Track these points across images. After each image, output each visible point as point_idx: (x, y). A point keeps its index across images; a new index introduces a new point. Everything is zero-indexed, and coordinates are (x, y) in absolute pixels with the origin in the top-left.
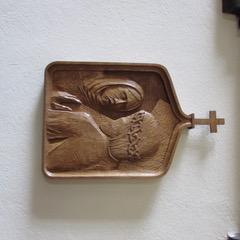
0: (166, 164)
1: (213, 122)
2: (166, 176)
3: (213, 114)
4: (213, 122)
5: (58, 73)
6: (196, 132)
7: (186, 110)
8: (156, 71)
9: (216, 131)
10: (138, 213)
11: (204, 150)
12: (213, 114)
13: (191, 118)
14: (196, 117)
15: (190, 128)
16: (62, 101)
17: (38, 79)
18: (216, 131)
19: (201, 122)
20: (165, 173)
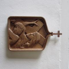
0: (43, 46)
1: (59, 34)
2: (43, 50)
3: (59, 32)
4: (59, 34)
5: (13, 21)
6: (52, 37)
7: (50, 30)
8: (43, 20)
9: (59, 37)
10: (36, 56)
11: (55, 41)
12: (59, 32)
13: (52, 34)
14: (53, 33)
15: (45, 27)
16: (29, 25)
17: (5, 23)
18: (59, 37)
19: (55, 34)
20: (43, 50)
